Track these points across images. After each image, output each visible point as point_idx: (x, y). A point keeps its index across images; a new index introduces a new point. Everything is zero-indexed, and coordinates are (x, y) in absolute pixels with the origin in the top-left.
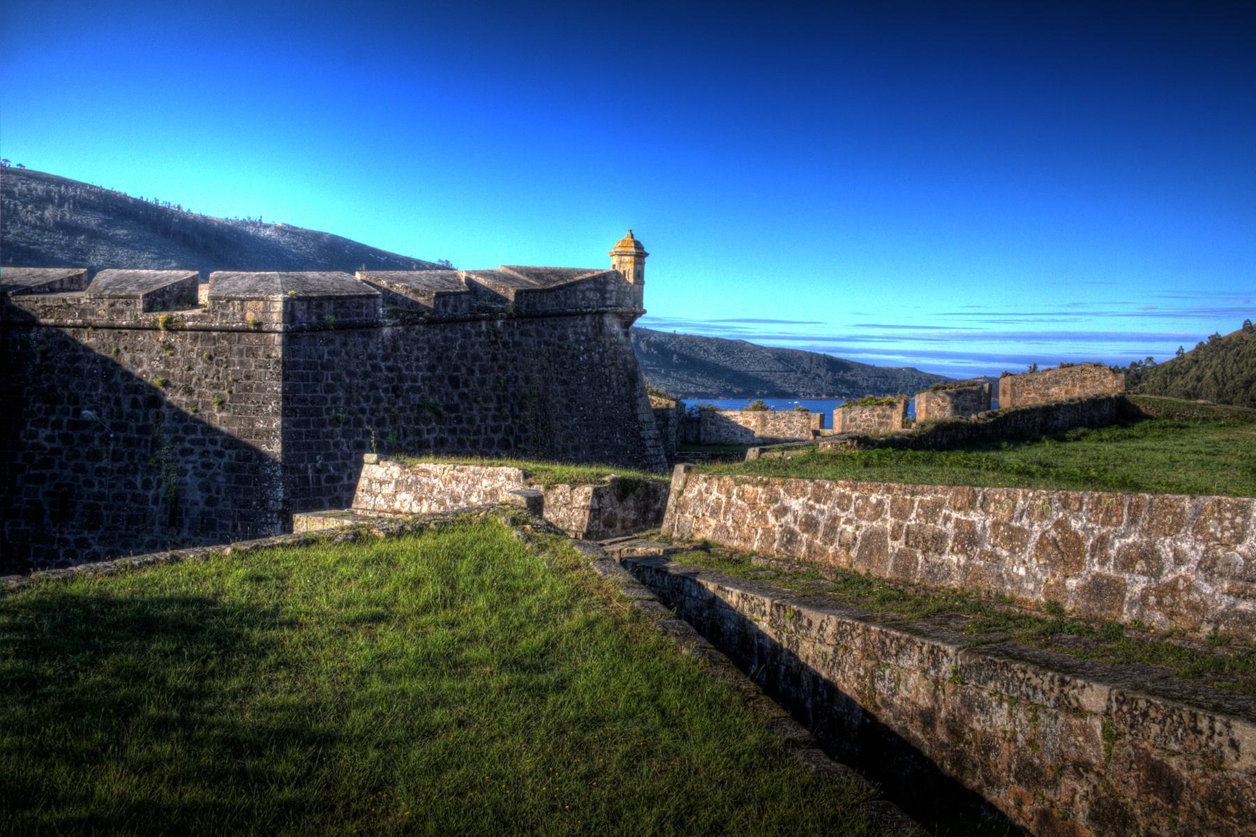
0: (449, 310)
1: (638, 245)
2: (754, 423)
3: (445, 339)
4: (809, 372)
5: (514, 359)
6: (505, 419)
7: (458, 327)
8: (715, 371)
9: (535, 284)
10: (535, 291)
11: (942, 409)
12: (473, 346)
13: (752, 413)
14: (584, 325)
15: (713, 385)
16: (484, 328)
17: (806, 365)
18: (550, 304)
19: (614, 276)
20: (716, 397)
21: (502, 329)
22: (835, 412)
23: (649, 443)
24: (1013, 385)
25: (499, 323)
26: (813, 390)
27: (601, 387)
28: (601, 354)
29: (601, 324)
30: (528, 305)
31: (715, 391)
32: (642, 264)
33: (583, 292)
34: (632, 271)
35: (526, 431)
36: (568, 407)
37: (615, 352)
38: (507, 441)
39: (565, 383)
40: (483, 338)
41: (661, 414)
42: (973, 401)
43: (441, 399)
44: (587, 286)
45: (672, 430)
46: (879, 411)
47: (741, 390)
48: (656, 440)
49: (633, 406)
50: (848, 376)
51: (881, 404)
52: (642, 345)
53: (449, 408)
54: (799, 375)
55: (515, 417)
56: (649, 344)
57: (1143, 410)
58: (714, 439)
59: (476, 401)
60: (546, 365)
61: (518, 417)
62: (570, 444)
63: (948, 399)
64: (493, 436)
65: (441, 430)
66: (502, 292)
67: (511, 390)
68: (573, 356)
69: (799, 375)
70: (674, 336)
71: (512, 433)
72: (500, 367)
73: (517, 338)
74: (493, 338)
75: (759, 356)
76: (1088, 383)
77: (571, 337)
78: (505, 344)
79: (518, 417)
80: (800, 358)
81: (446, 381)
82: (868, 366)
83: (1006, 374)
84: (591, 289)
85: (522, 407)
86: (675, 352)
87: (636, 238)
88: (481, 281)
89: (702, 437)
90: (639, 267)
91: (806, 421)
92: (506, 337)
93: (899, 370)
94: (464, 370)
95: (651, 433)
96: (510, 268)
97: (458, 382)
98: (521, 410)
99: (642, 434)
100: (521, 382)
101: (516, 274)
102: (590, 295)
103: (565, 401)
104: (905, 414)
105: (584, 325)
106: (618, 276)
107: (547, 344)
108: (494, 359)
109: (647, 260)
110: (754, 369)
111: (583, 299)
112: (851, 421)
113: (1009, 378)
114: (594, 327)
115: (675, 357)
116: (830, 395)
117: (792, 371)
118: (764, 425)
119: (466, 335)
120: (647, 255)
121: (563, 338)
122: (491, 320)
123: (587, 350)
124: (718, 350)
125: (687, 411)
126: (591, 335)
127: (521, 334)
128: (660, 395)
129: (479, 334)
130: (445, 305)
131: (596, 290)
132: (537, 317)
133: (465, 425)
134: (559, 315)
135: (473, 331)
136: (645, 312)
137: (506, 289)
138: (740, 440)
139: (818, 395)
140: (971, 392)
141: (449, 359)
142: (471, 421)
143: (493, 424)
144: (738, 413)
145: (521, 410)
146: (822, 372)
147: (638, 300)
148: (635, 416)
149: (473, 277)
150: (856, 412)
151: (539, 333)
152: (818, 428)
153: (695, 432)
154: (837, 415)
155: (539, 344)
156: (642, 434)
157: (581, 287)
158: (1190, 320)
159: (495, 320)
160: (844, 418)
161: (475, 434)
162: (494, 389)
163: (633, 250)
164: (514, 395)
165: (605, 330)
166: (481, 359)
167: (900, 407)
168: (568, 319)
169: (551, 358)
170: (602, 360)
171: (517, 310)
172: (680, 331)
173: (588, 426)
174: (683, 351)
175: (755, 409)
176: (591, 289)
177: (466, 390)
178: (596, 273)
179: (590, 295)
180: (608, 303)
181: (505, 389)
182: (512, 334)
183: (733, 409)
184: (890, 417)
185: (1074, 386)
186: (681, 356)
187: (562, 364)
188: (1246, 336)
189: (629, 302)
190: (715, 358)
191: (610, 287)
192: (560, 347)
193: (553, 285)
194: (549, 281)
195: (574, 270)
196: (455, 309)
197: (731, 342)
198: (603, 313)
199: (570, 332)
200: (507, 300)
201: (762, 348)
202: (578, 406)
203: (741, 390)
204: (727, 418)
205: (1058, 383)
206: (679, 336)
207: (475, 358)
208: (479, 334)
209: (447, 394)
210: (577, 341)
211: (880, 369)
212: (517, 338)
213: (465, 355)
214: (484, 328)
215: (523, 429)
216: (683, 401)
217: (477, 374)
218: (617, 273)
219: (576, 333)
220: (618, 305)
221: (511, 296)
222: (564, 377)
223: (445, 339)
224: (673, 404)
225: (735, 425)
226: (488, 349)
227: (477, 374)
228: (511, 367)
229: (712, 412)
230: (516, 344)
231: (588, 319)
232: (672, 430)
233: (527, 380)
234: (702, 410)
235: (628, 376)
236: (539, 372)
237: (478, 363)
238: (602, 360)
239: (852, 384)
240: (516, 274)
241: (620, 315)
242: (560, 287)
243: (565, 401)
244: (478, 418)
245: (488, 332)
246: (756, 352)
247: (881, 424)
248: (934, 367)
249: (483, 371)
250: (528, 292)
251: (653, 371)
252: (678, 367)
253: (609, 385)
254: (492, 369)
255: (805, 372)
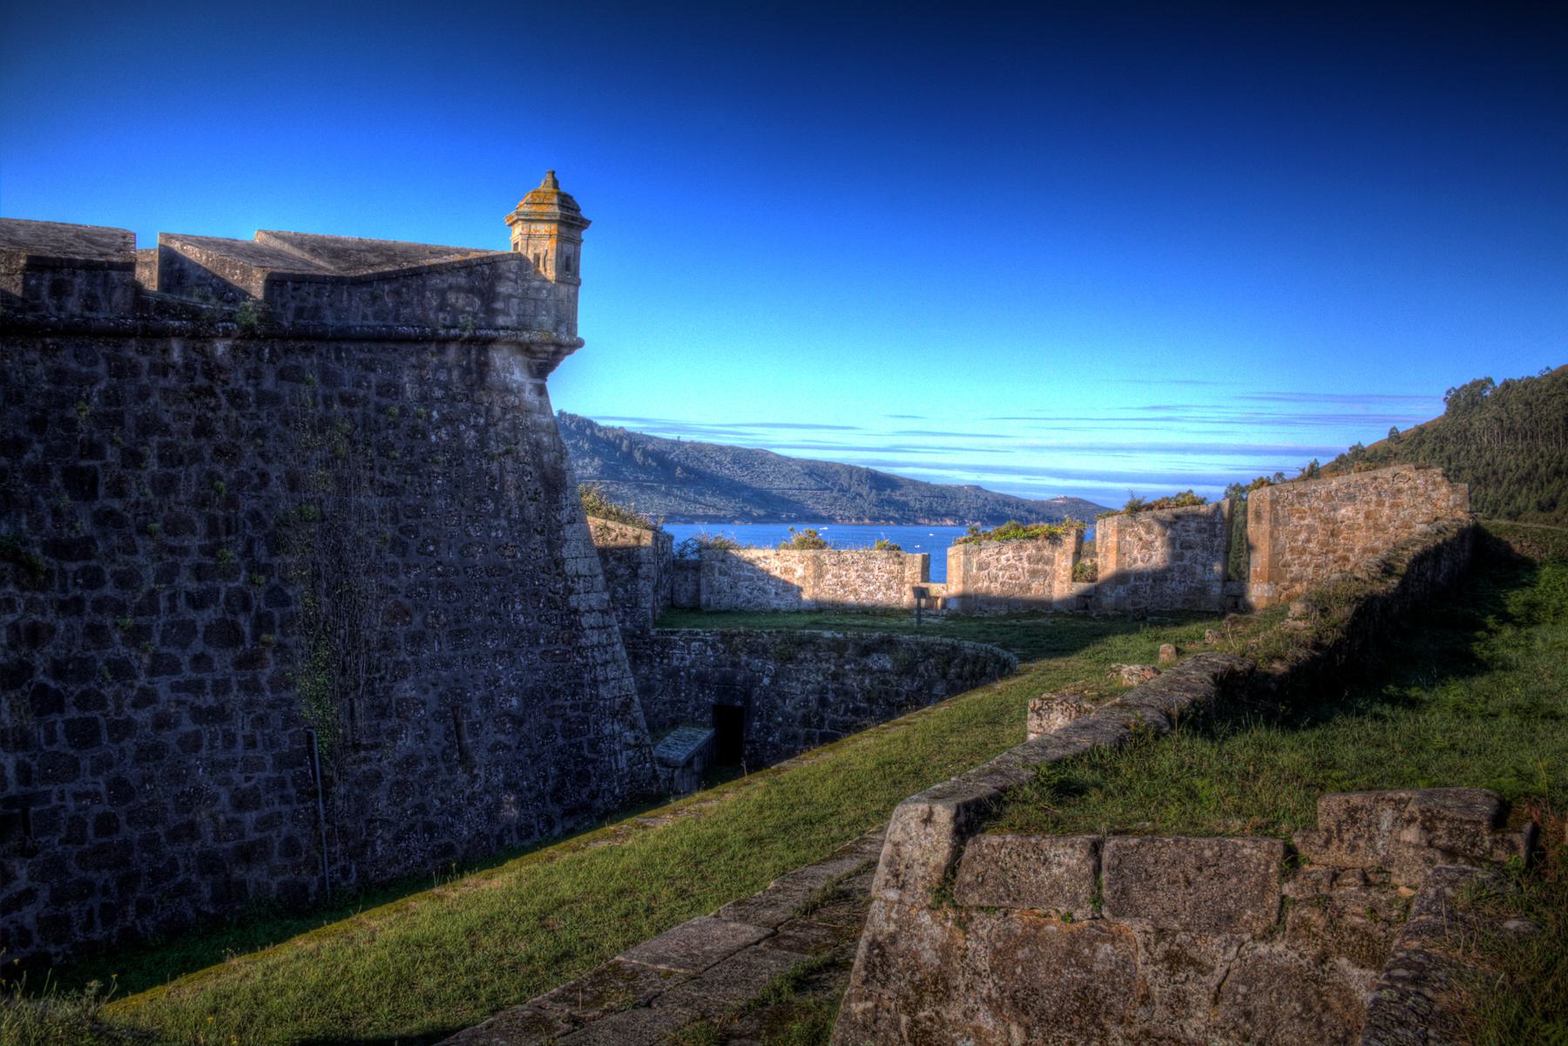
0: (73, 305)
1: (566, 202)
2: (800, 572)
3: (59, 376)
4: (848, 491)
5: (261, 433)
6: (230, 574)
7: (102, 349)
8: (729, 489)
9: (324, 266)
10: (320, 281)
11: (1148, 545)
12: (143, 395)
13: (796, 553)
14: (442, 365)
15: (727, 506)
16: (176, 355)
17: (844, 480)
18: (358, 314)
19: (513, 264)
20: (731, 521)
21: (227, 361)
22: (950, 551)
23: (587, 620)
24: (1274, 502)
25: (221, 347)
26: (852, 513)
27: (480, 500)
28: (482, 431)
29: (483, 367)
30: (299, 312)
31: (730, 514)
32: (577, 243)
33: (442, 293)
34: (552, 256)
35: (286, 602)
36: (399, 546)
37: (514, 427)
38: (234, 626)
39: (390, 490)
40: (172, 380)
41: (619, 561)
42: (1200, 530)
43: (37, 525)
44: (452, 280)
45: (646, 587)
46: (1030, 549)
47: (762, 512)
48: (604, 612)
49: (554, 541)
50: (897, 496)
51: (1035, 537)
52: (637, 455)
53: (59, 549)
54: (835, 494)
55: (256, 568)
56: (646, 454)
57: (1517, 548)
58: (726, 602)
59: (143, 530)
60: (343, 448)
61: (265, 569)
62: (400, 630)
63: (1157, 528)
64: (191, 615)
65: (31, 605)
66: (235, 278)
67: (247, 504)
68: (414, 432)
69: (835, 494)
70: (677, 444)
71: (246, 607)
72: (218, 451)
73: (269, 383)
74: (201, 381)
75: (785, 470)
76: (1405, 498)
77: (410, 390)
78: (236, 398)
79: (265, 569)
80: (837, 472)
81: (56, 481)
82: (922, 484)
83: (1261, 483)
84: (459, 289)
85: (276, 545)
86: (679, 464)
87: (563, 189)
88: (193, 253)
89: (704, 597)
90: (569, 248)
91: (895, 568)
92: (238, 380)
93: (960, 488)
94: (112, 454)
95: (593, 600)
96: (277, 236)
97: (94, 482)
98: (273, 553)
99: (573, 601)
100: (276, 487)
101: (286, 247)
102: (458, 300)
103: (389, 531)
104: (1078, 554)
105: (442, 365)
106: (523, 266)
107: (346, 400)
108: (203, 429)
109: (585, 234)
110: (778, 485)
111: (441, 308)
112: (981, 567)
113: (1267, 490)
114: (467, 371)
115: (679, 470)
116: (875, 519)
117: (826, 488)
118: (819, 575)
119: (121, 370)
120: (584, 224)
121: (391, 389)
122: (199, 335)
123: (446, 420)
124: (734, 462)
125: (676, 550)
126: (458, 388)
127: (281, 376)
128: (624, 520)
129: (163, 370)
130: (59, 290)
131: (471, 290)
132: (321, 338)
133: (109, 590)
134: (380, 339)
135: (145, 361)
136: (579, 344)
137: (246, 272)
138: (775, 603)
139: (859, 519)
140: (1196, 516)
141: (70, 425)
142: (126, 580)
143: (193, 586)
144: (772, 552)
145: (273, 553)
146: (865, 490)
147: (567, 319)
148: (559, 563)
149: (176, 245)
150: (989, 552)
151: (328, 377)
152: (919, 583)
153: (691, 588)
154: (955, 557)
155: (327, 401)
156: (573, 601)
157: (435, 281)
158: (1292, 429)
159: (209, 338)
160: (968, 563)
161: (139, 611)
162: (201, 502)
163: (556, 210)
164: (255, 516)
165: (493, 378)
166: (166, 430)
167: (1070, 542)
168: (403, 349)
169: (358, 435)
170: (482, 443)
171: (268, 317)
172: (686, 438)
173: (447, 588)
174: (694, 465)
175: (802, 545)
176: (459, 289)
177: (117, 504)
178: (472, 256)
179: (458, 300)
180: (501, 321)
181: (231, 502)
182: (255, 375)
183: (761, 543)
184: (1050, 561)
185: (1380, 504)
186: (686, 469)
187: (384, 449)
188: (1393, 446)
189: (546, 320)
190: (728, 471)
191: (504, 288)
192: (381, 410)
193: (364, 272)
194: (359, 263)
195: (416, 248)
196: (91, 302)
197: (750, 451)
198: (492, 341)
199: (407, 380)
200: (245, 294)
201: (788, 459)
202: (424, 544)
203: (762, 512)
204: (750, 562)
205: (1352, 498)
206: (684, 443)
207: (148, 426)
208: (163, 370)
209: (56, 513)
210: (424, 399)
211: (935, 487)
212: (269, 383)
213: (118, 419)
214: (176, 355)
215: (278, 597)
216: (669, 529)
217: (153, 465)
218: (521, 259)
219: (421, 381)
220: (523, 327)
221: (257, 288)
222: (391, 478)
223: (59, 376)
224: (647, 539)
225: (766, 576)
226: (186, 407)
227: (153, 465)
228: (249, 450)
229: (722, 552)
230: (263, 398)
231: (452, 353)
232: (646, 587)
233: (293, 483)
234: (703, 548)
235: (544, 478)
236: (328, 464)
237: (155, 440)
238: (482, 443)
239: (902, 506)
240: (286, 247)
241: (527, 349)
242: (384, 278)
243: (389, 531)
244: (150, 573)
245: (188, 366)
246: (783, 464)
247: (1034, 574)
248: (1003, 486)
249: (169, 457)
250: (300, 280)
251: (651, 488)
252: (684, 483)
253: (498, 497)
254: (196, 456)
255: (843, 490)
